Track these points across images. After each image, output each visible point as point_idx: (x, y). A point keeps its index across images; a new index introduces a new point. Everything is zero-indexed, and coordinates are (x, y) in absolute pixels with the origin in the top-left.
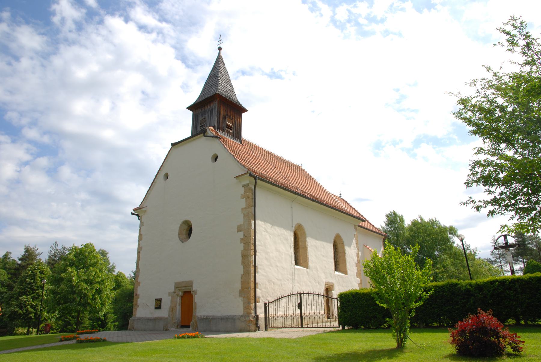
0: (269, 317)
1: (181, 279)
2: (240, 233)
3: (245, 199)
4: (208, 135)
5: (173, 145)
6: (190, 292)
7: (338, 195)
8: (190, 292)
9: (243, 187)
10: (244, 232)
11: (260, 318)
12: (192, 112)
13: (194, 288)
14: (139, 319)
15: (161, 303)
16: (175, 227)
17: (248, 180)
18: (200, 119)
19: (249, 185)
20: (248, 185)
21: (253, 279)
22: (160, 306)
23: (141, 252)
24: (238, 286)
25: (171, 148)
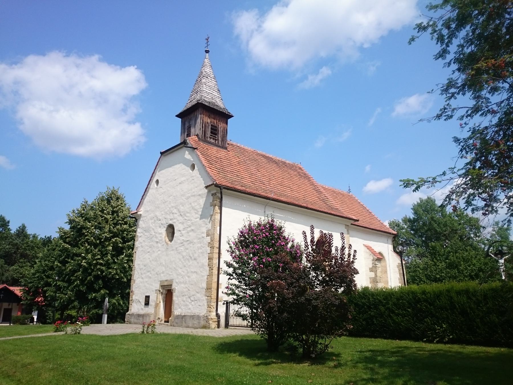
0: (229, 316)
1: (164, 278)
2: (208, 237)
3: (212, 207)
4: (188, 146)
5: (162, 153)
6: (171, 289)
7: (345, 191)
8: (171, 289)
9: (212, 196)
10: (211, 237)
11: (221, 316)
12: (180, 119)
13: (173, 287)
14: (132, 315)
15: (149, 300)
16: (163, 231)
17: (215, 190)
18: (187, 125)
19: (216, 194)
20: (215, 194)
21: (216, 280)
22: (149, 302)
23: (137, 252)
24: (204, 285)
25: (161, 156)
